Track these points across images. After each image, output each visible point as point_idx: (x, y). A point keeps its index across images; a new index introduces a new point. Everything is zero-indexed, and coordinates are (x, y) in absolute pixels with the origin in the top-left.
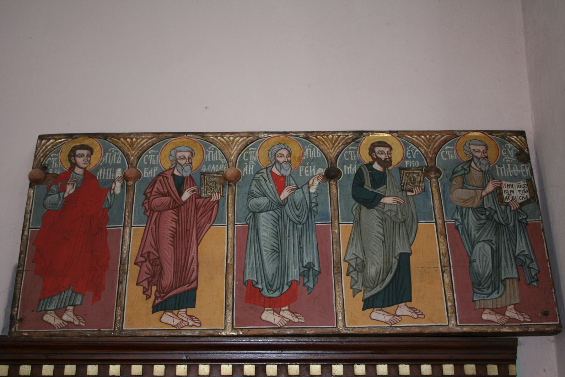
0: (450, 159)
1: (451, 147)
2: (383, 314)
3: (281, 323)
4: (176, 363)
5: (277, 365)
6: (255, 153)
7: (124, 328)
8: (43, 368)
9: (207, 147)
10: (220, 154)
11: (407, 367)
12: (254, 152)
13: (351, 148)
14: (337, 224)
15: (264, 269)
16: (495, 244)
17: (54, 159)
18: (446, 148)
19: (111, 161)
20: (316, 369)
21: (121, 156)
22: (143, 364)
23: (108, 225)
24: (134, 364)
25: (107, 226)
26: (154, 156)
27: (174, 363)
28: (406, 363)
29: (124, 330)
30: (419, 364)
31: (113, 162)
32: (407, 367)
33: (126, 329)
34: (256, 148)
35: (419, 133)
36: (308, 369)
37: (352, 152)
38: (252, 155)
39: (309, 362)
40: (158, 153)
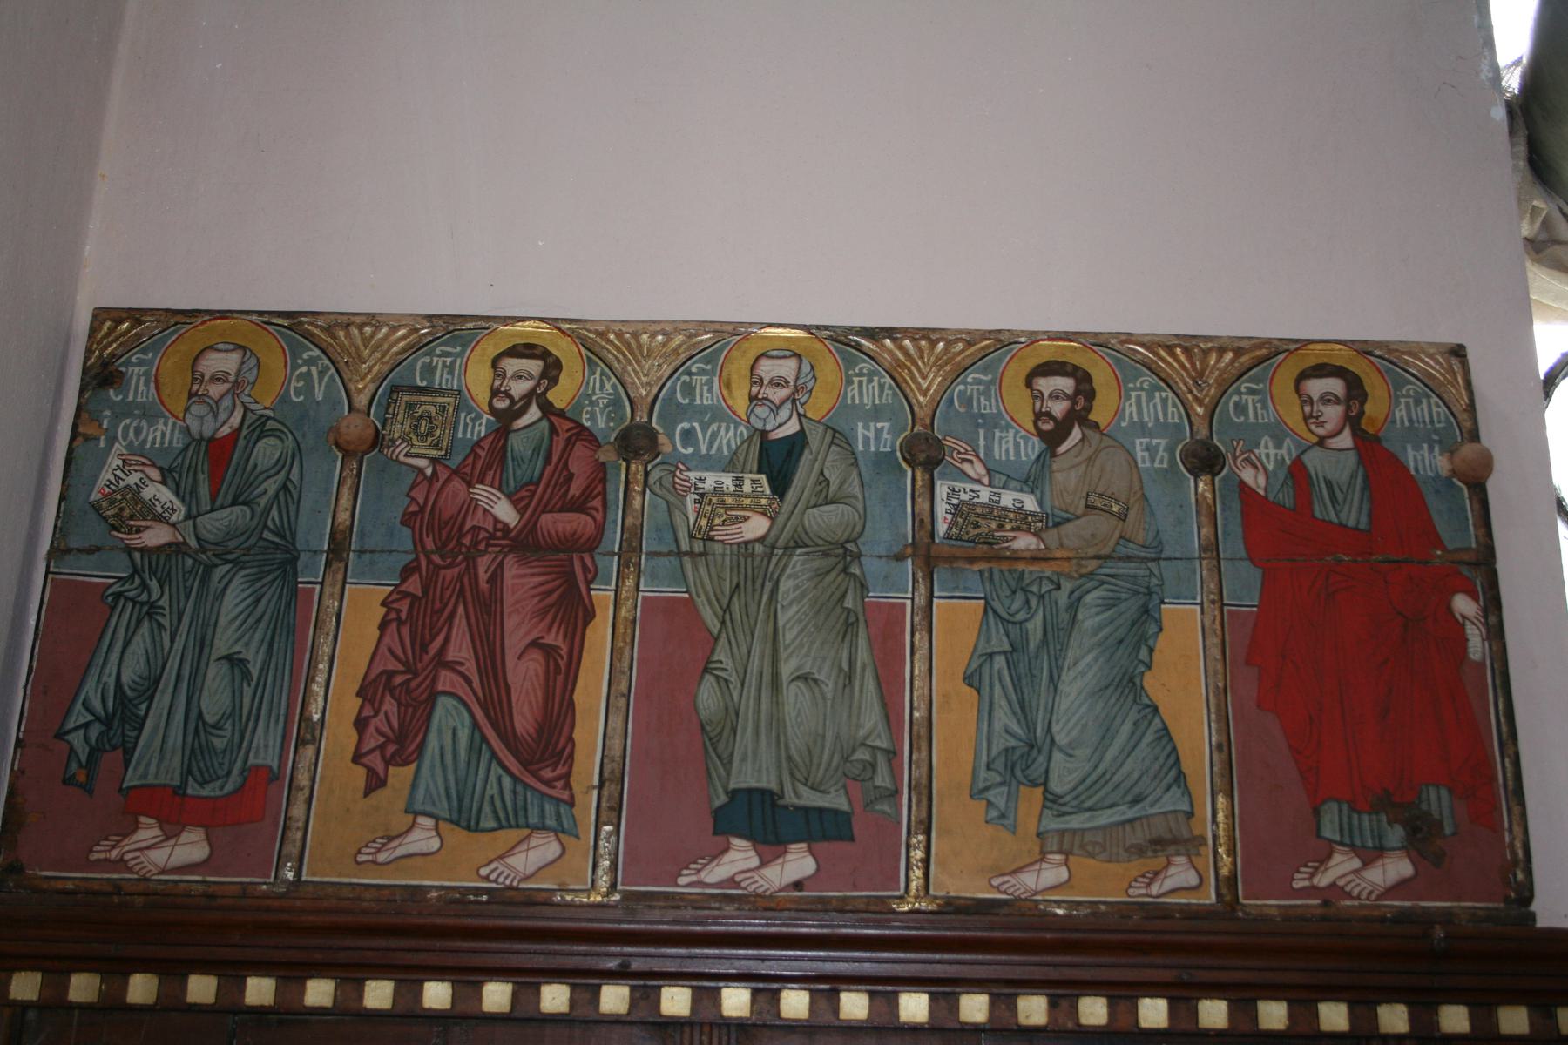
0: (698, 402)
1: (986, 375)
2: (174, 846)
3: (502, 873)
4: (1135, 993)
5: (752, 989)
6: (453, 363)
7: (304, 878)
8: (367, 988)
9: (850, 362)
10: (1438, 406)
11: (1162, 1004)
12: (449, 360)
13: (973, 378)
14: (917, 600)
15: (174, 708)
16: (565, 657)
17: (699, 378)
18: (969, 380)
19: (1149, 416)
20: (795, 1003)
21: (890, 388)
22: (453, 978)
23: (1252, 612)
24: (1089, 995)
25: (299, 580)
26: (704, 378)
27: (414, 977)
28: (443, 977)
29: (306, 882)
30: (414, 981)
31: (874, 401)
32: (1162, 1004)
33: (310, 879)
34: (459, 349)
35: (1168, 345)
36: (955, 1008)
37: (1250, 398)
38: (443, 371)
39: (602, 978)
40: (992, 382)
